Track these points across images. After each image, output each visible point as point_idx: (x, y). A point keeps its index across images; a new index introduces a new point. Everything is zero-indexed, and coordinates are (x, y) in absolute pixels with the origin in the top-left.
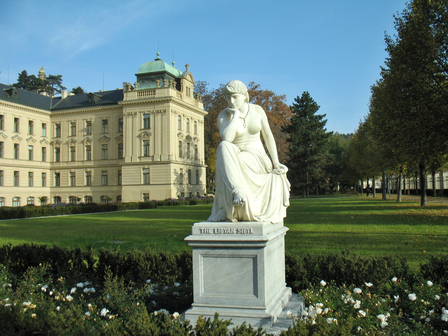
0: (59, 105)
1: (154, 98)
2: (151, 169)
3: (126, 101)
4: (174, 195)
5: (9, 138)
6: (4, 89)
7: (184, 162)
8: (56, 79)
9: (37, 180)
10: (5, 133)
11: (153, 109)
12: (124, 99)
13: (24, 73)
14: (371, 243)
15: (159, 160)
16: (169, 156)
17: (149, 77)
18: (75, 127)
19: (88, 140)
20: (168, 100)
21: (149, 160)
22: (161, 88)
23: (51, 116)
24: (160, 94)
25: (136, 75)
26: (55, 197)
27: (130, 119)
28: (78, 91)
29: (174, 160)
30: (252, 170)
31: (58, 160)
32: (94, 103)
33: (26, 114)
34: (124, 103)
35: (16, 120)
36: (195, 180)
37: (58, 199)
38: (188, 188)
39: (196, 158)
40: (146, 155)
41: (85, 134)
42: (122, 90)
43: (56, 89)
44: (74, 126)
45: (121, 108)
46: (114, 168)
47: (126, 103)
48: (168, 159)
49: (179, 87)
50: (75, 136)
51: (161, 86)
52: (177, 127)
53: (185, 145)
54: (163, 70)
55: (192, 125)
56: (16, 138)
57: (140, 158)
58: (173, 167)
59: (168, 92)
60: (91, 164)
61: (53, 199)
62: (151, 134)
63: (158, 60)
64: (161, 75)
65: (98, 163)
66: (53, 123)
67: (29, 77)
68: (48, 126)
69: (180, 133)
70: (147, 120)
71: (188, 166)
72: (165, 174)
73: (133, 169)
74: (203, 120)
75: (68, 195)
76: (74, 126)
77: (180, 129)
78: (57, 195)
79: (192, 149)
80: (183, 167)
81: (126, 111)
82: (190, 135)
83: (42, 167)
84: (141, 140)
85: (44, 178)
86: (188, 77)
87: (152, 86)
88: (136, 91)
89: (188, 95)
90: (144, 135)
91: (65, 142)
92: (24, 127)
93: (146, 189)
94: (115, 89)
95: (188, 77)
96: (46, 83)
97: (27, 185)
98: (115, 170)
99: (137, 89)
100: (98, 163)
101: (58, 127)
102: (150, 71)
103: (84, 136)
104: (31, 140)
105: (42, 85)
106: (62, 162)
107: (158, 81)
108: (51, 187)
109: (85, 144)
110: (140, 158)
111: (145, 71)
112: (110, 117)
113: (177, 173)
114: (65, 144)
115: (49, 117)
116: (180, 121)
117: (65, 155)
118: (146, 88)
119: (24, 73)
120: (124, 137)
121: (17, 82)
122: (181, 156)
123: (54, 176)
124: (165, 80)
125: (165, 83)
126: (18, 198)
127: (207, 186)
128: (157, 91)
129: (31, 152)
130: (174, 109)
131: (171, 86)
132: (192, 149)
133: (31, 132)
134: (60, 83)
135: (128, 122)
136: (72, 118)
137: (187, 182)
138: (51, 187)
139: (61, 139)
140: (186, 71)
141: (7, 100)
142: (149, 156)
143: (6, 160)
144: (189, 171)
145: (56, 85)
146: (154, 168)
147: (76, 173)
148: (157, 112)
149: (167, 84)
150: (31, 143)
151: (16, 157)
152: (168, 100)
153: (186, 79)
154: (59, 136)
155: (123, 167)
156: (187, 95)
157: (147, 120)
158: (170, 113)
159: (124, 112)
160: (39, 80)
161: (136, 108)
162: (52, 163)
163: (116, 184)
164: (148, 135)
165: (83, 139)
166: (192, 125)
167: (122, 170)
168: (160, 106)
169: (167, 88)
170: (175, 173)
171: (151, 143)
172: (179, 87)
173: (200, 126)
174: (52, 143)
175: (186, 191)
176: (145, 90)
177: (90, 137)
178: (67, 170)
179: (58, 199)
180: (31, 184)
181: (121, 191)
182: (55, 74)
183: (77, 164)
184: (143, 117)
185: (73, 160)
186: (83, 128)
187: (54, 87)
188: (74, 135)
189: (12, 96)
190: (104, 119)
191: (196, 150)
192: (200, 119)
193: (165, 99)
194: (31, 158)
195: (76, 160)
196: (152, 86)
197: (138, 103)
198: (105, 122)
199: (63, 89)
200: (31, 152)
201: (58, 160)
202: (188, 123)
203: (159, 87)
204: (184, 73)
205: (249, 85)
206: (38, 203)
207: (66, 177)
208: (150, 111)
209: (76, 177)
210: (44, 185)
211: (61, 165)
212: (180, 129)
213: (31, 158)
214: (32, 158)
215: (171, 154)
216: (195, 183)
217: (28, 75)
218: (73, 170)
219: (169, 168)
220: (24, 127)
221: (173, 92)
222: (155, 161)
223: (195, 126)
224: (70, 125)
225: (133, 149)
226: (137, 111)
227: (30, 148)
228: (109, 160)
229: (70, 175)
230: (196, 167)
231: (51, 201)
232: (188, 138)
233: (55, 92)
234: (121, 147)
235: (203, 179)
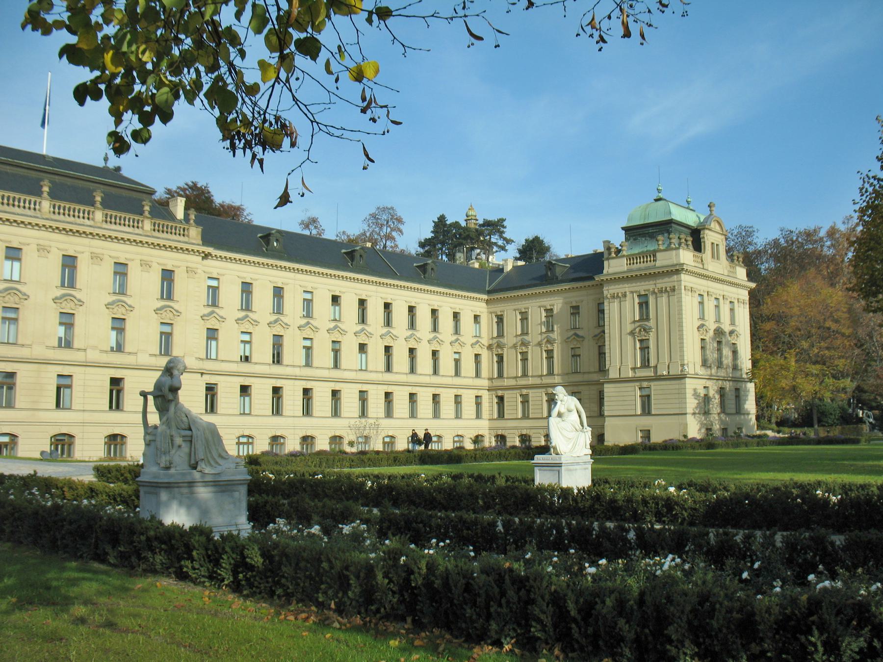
0: (499, 283)
1: (654, 267)
3: (608, 274)
4: (694, 431)
5: (425, 342)
7: (711, 375)
8: (496, 226)
9: (468, 407)
10: (418, 334)
11: (653, 286)
12: (605, 272)
13: (442, 219)
15: (665, 373)
16: (682, 365)
17: (645, 231)
18: (527, 319)
20: (677, 270)
21: (649, 373)
23: (488, 302)
24: (663, 260)
25: (623, 228)
26: (497, 436)
27: (615, 305)
28: (533, 249)
29: (691, 371)
30: (294, 366)
31: (500, 375)
32: (557, 278)
33: (448, 302)
34: (604, 278)
35: (434, 312)
36: (734, 406)
37: (501, 438)
38: (720, 419)
39: (735, 368)
40: (645, 363)
41: (544, 330)
42: (602, 253)
43: (495, 244)
44: (524, 318)
45: (601, 285)
47: (609, 278)
48: (682, 371)
49: (698, 246)
50: (527, 334)
51: (666, 246)
52: (697, 315)
53: (712, 346)
55: (725, 309)
56: (435, 342)
57: (634, 369)
58: (691, 385)
59: (678, 255)
61: (493, 439)
62: (650, 328)
66: (491, 313)
67: (451, 225)
68: (484, 320)
69: (702, 326)
71: (720, 382)
72: (677, 396)
73: (613, 390)
74: (747, 298)
75: (518, 433)
76: (524, 318)
77: (702, 318)
78: (500, 432)
79: (727, 352)
80: (709, 383)
81: (608, 290)
82: (723, 327)
83: (475, 386)
84: (635, 339)
85: (478, 404)
86: (714, 225)
87: (651, 246)
88: (623, 256)
89: (715, 256)
91: (510, 344)
92: (446, 322)
93: (646, 422)
94: (590, 251)
95: (714, 225)
96: (479, 233)
97: (453, 415)
98: (594, 390)
99: (625, 253)
101: (500, 319)
102: (647, 222)
103: (541, 333)
104: (457, 344)
105: (472, 239)
106: (508, 378)
107: (660, 237)
109: (544, 348)
110: (634, 369)
113: (699, 396)
114: (511, 348)
115: (484, 305)
116: (701, 303)
117: (513, 366)
118: (641, 250)
119: (442, 219)
120: (607, 335)
121: (430, 235)
122: (705, 363)
123: (495, 400)
124: (671, 236)
125: (673, 241)
127: (758, 418)
128: (658, 255)
129: (457, 362)
130: (689, 285)
131: (683, 245)
132: (727, 352)
133: (457, 331)
134: (503, 232)
135: (612, 309)
136: (522, 305)
137: (719, 410)
139: (504, 340)
140: (711, 215)
141: (420, 282)
142: (648, 366)
143: (257, 366)
144: (722, 391)
145: (496, 237)
146: (659, 388)
147: (530, 395)
148: (661, 291)
149: (675, 241)
151: (388, 368)
152: (677, 270)
153: (710, 230)
154: (501, 334)
155: (605, 386)
156: (713, 257)
157: (644, 305)
158: (683, 291)
159: (605, 292)
160: (466, 229)
162: (491, 379)
164: (646, 330)
166: (725, 309)
167: (605, 390)
168: (666, 280)
169: (676, 249)
170: (696, 394)
171: (652, 345)
172: (698, 246)
173: (741, 309)
174: (490, 347)
175: (717, 427)
176: (639, 253)
179: (501, 438)
180: (458, 415)
181: (603, 427)
182: (493, 218)
183: (531, 381)
184: (637, 300)
185: (525, 375)
187: (493, 240)
188: (525, 333)
190: (574, 304)
191: (735, 352)
192: (740, 297)
194: (457, 373)
195: (530, 374)
198: (575, 310)
199: (508, 243)
200: (457, 362)
201: (500, 375)
202: (717, 307)
203: (661, 247)
204: (706, 220)
205: (844, 223)
206: (469, 446)
207: (513, 402)
208: (648, 290)
209: (531, 403)
210: (478, 416)
211: (506, 383)
212: (702, 318)
213: (457, 373)
214: (121, 407)
215: (686, 362)
216: (734, 411)
217: (448, 223)
218: (524, 392)
219: (683, 386)
220: (446, 322)
221: (686, 256)
223: (732, 310)
224: (519, 317)
226: (627, 290)
227: (457, 356)
228: (584, 373)
229: (520, 399)
230: (735, 383)
231: (489, 442)
232: (719, 332)
233: (495, 249)
234: (602, 354)
235: (750, 405)
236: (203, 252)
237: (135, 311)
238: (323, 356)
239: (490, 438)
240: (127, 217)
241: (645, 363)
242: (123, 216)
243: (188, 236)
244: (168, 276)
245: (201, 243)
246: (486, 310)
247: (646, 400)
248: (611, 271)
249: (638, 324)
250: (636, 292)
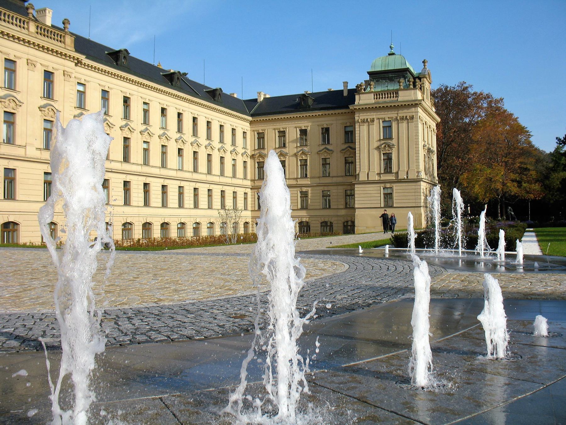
2: (394, 188)
6: (161, 73)
12: (356, 103)
14: (547, 299)
16: (418, 172)
17: (386, 75)
18: (263, 138)
19: (304, 153)
21: (391, 177)
22: (404, 90)
23: (251, 123)
24: (404, 96)
27: (365, 128)
32: (309, 107)
34: (357, 108)
40: (388, 168)
41: (299, 145)
44: (282, 134)
45: (353, 113)
46: (340, 187)
48: (417, 176)
50: (264, 148)
54: (405, 67)
57: (379, 174)
59: (415, 94)
60: (307, 182)
63: (393, 54)
64: (403, 73)
65: (317, 181)
66: (254, 131)
70: (388, 129)
74: (435, 128)
76: (282, 134)
81: (359, 117)
84: (380, 153)
87: (392, 87)
90: (385, 146)
94: (326, 90)
100: (317, 181)
103: (297, 147)
108: (252, 211)
110: (379, 174)
111: (378, 69)
112: (332, 124)
118: (382, 89)
126: (183, 224)
128: (400, 93)
129: (146, 151)
135: (361, 132)
136: (281, 126)
138: (252, 211)
142: (391, 172)
146: (399, 188)
148: (402, 119)
150: (165, 142)
157: (388, 129)
159: (356, 118)
161: (372, 114)
162: (253, 181)
163: (342, 207)
165: (295, 152)
167: (356, 189)
168: (405, 111)
174: (252, 157)
177: (305, 148)
178: (295, 189)
186: (295, 138)
189: (216, 99)
190: (325, 126)
193: (414, 103)
194: (146, 162)
196: (396, 87)
197: (376, 107)
198: (326, 131)
208: (392, 118)
222: (399, 178)
225: (368, 163)
228: (333, 177)
236: (78, 59)
237: (23, 105)
238: (155, 158)
239: (252, 225)
240: (15, 16)
241: (388, 168)
242: (11, 15)
243: (64, 43)
244: (48, 76)
245: (74, 50)
246: (249, 129)
247: (388, 196)
248: (361, 102)
249: (383, 142)
250: (277, 129)
